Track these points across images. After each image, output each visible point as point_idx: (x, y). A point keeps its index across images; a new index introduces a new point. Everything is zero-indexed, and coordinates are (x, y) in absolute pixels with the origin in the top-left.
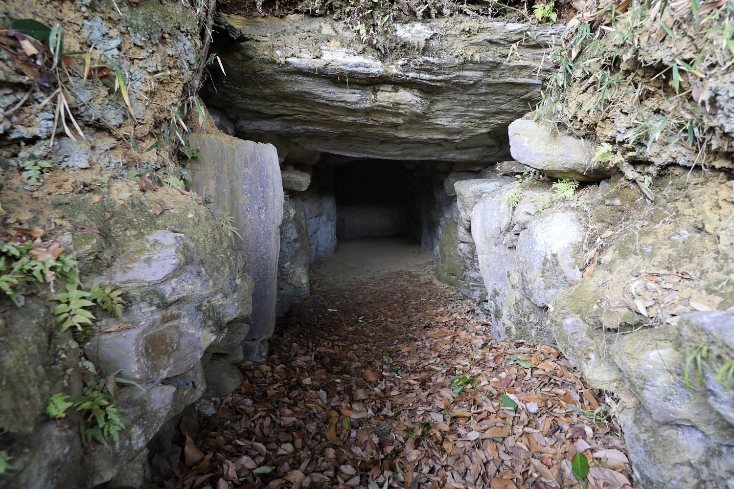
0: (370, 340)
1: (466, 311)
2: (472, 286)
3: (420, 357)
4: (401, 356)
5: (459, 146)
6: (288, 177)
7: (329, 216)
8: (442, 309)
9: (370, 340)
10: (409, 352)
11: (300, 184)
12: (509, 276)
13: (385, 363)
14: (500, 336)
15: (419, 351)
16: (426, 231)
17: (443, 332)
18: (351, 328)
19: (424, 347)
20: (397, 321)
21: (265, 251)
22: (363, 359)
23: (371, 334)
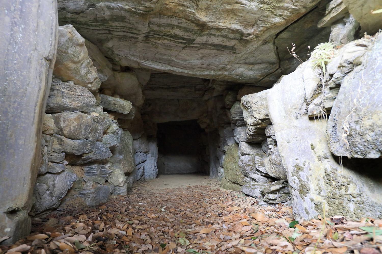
0: (169, 224)
1: (251, 204)
2: (253, 185)
3: (220, 239)
4: (199, 237)
5: (247, 61)
6: (114, 100)
7: (153, 154)
8: (231, 203)
9: (169, 224)
10: (207, 234)
11: (123, 107)
12: (313, 149)
13: (181, 246)
14: (308, 213)
15: (217, 233)
16: (212, 164)
17: (238, 217)
18: (153, 215)
19: (222, 230)
20: (195, 211)
21: (19, 83)
22: (157, 241)
23: (171, 220)
